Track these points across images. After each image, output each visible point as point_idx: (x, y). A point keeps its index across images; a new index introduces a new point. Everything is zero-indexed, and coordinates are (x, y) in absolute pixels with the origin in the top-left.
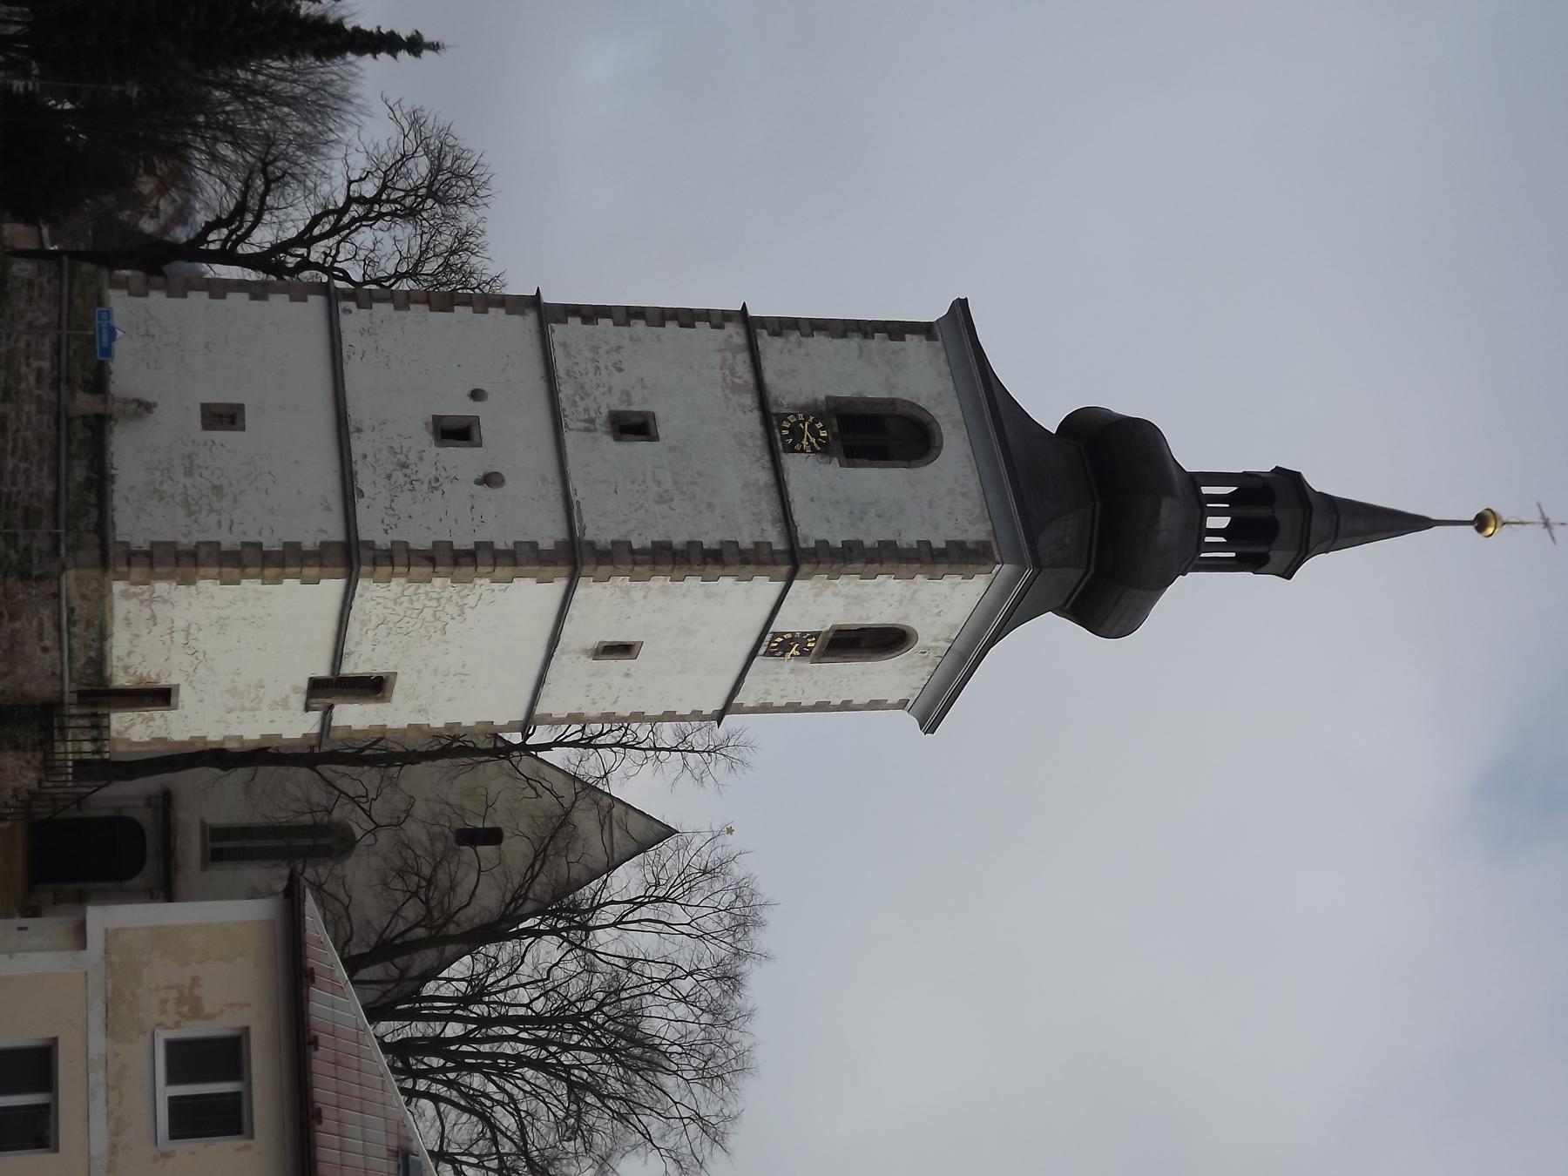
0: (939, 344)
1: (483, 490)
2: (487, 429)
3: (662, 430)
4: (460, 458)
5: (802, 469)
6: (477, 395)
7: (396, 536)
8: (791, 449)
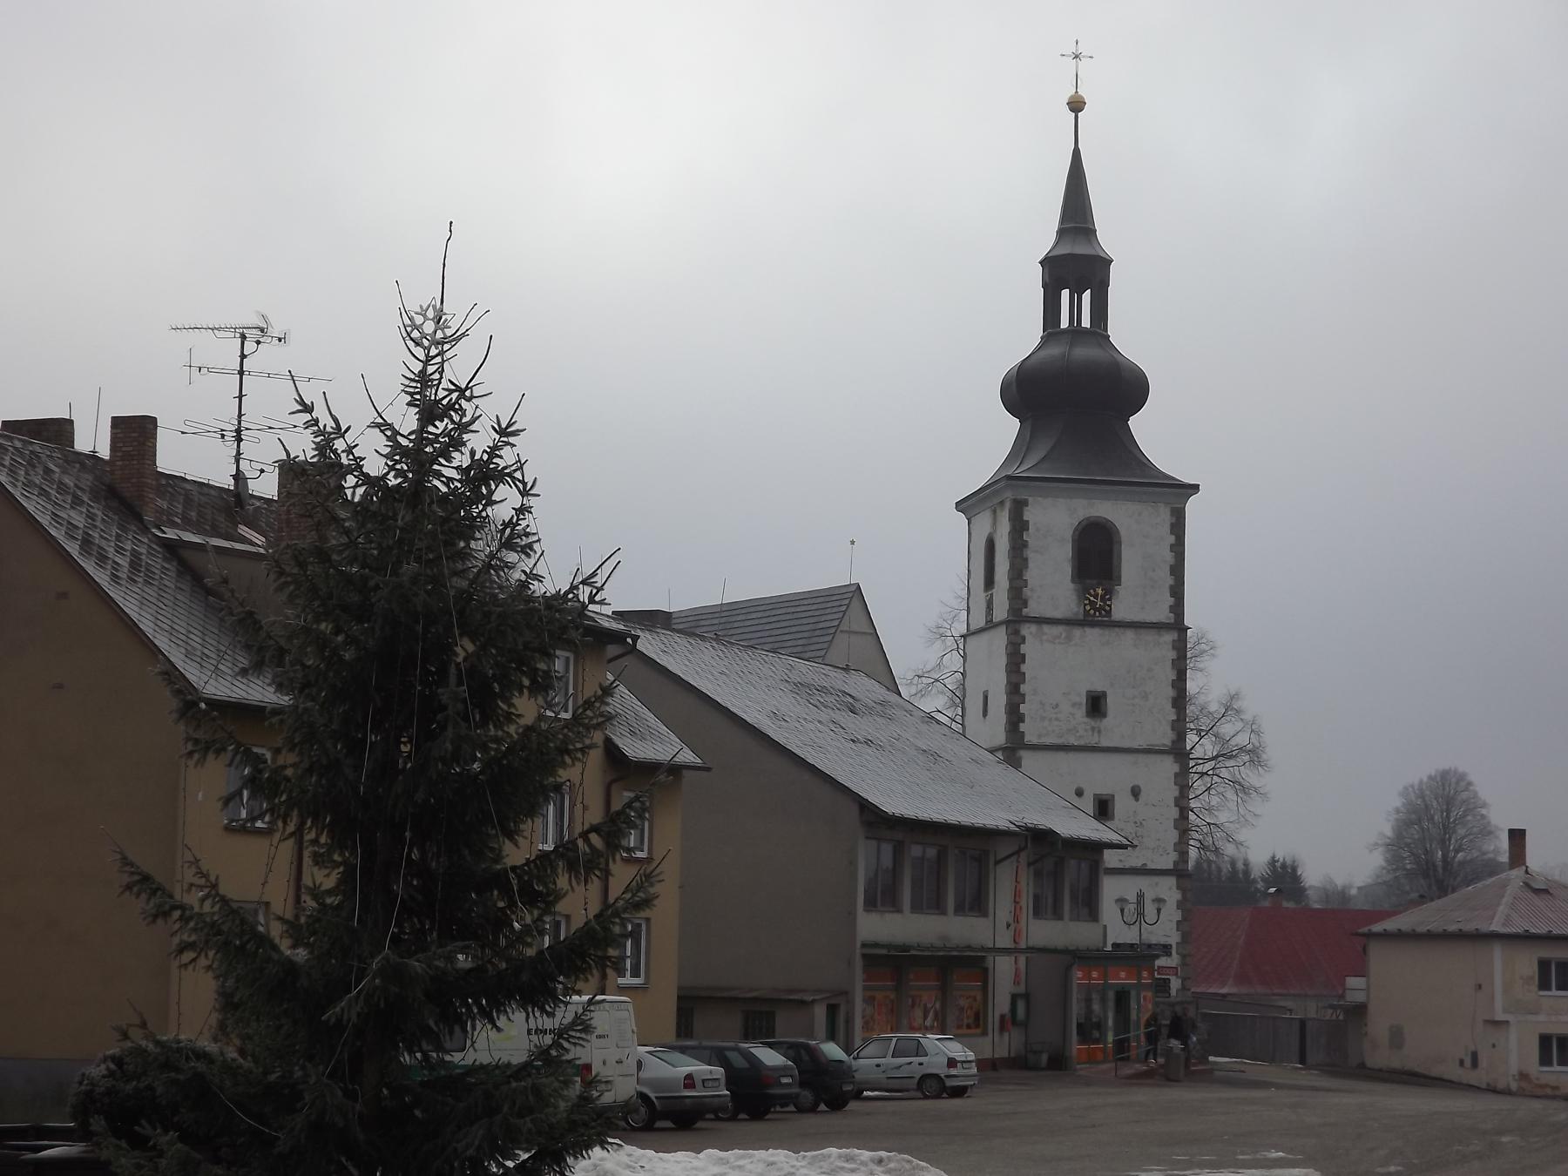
0: (1030, 500)
1: (1143, 797)
2: (1103, 791)
3: (1099, 688)
4: (1122, 805)
5: (1122, 608)
6: (1079, 793)
7: (1171, 848)
8: (1109, 613)
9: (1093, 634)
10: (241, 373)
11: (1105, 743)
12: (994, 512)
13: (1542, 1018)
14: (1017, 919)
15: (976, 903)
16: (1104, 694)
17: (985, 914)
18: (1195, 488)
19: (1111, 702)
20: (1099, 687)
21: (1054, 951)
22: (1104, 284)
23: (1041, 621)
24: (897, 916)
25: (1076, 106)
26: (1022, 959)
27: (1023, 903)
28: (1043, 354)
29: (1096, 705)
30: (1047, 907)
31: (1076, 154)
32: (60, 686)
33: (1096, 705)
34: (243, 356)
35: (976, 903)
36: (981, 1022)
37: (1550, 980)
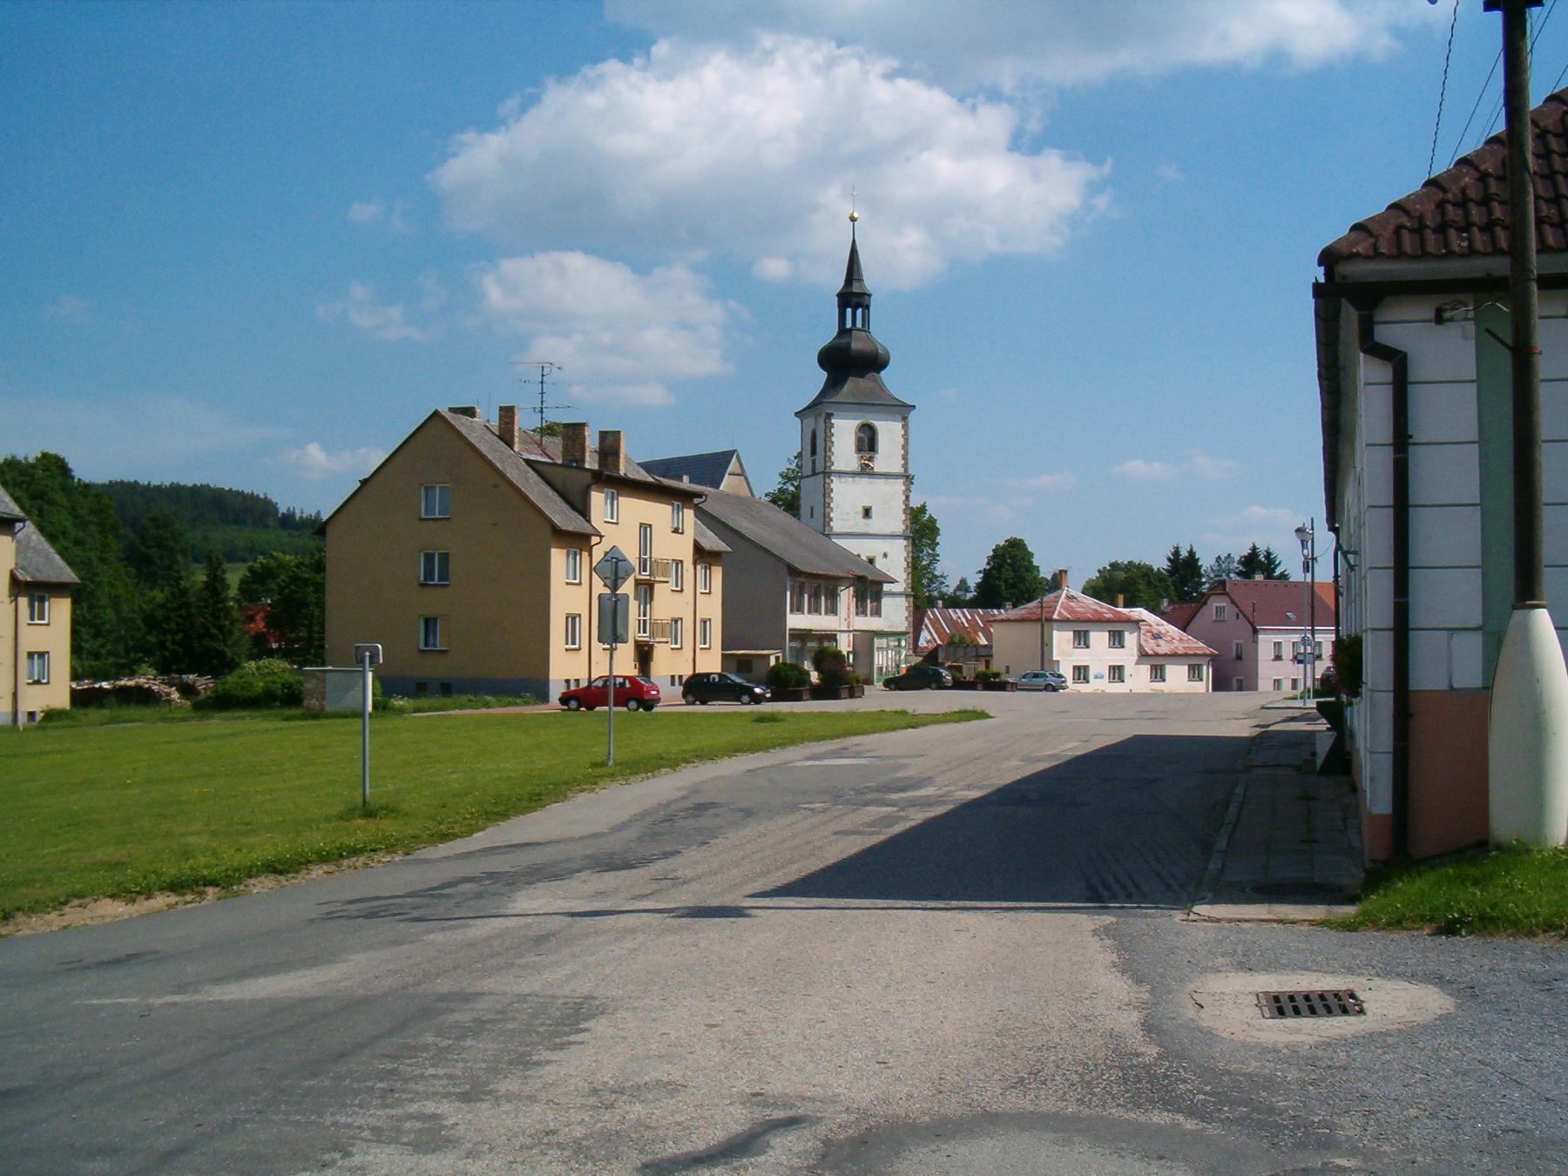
5: (879, 465)
9: (865, 481)
10: (542, 383)
11: (870, 532)
12: (816, 419)
13: (1074, 658)
14: (849, 617)
15: (833, 610)
16: (871, 508)
17: (836, 615)
18: (914, 406)
19: (874, 512)
20: (867, 504)
21: (871, 631)
22: (867, 307)
23: (841, 474)
24: (802, 616)
25: (853, 219)
26: (851, 635)
27: (851, 609)
28: (837, 341)
29: (867, 513)
30: (861, 611)
31: (854, 241)
32: (496, 524)
33: (867, 513)
34: (543, 376)
35: (833, 610)
36: (1310, 569)
37: (278, 1009)
